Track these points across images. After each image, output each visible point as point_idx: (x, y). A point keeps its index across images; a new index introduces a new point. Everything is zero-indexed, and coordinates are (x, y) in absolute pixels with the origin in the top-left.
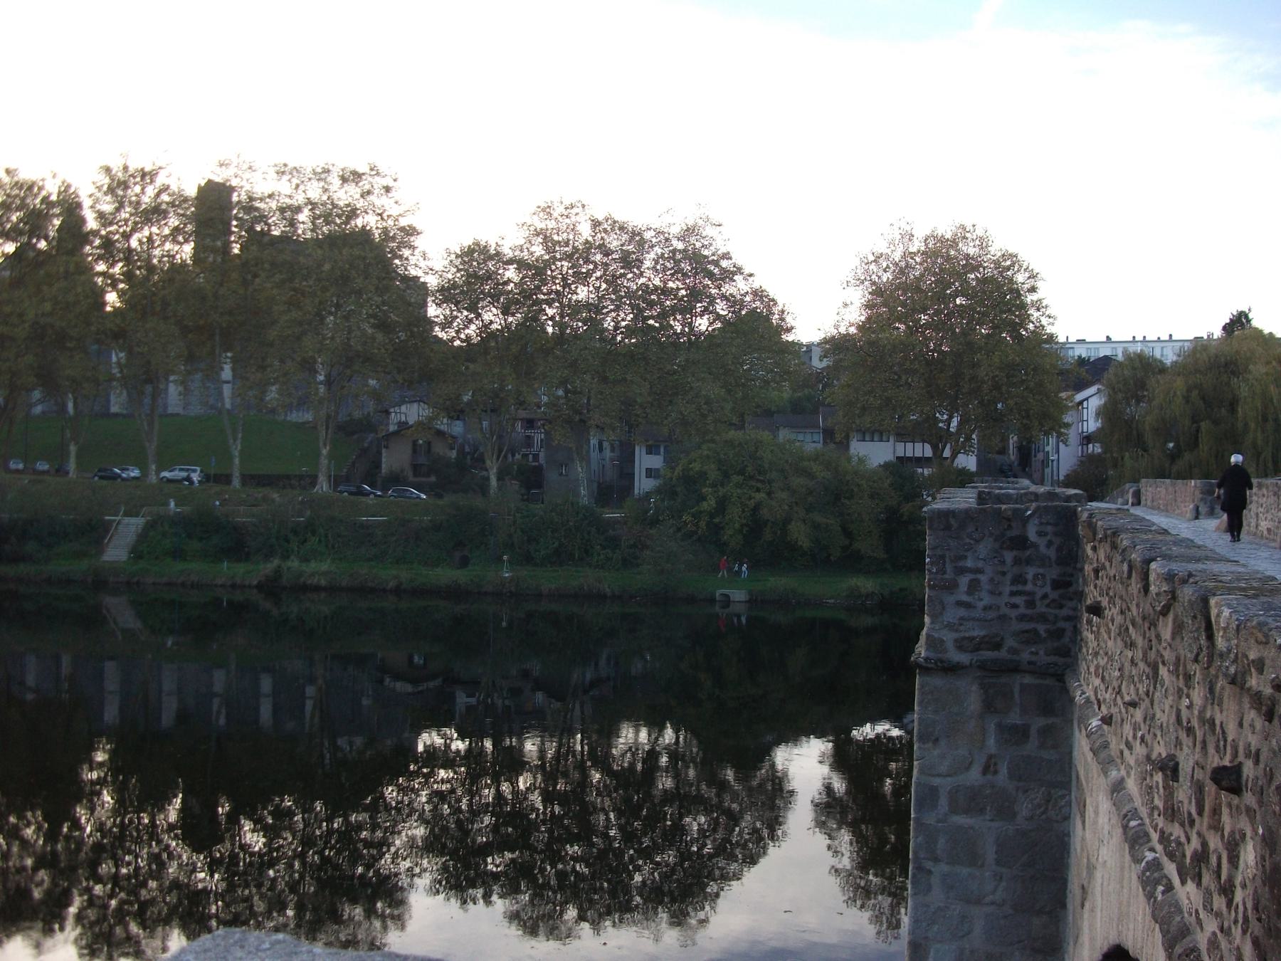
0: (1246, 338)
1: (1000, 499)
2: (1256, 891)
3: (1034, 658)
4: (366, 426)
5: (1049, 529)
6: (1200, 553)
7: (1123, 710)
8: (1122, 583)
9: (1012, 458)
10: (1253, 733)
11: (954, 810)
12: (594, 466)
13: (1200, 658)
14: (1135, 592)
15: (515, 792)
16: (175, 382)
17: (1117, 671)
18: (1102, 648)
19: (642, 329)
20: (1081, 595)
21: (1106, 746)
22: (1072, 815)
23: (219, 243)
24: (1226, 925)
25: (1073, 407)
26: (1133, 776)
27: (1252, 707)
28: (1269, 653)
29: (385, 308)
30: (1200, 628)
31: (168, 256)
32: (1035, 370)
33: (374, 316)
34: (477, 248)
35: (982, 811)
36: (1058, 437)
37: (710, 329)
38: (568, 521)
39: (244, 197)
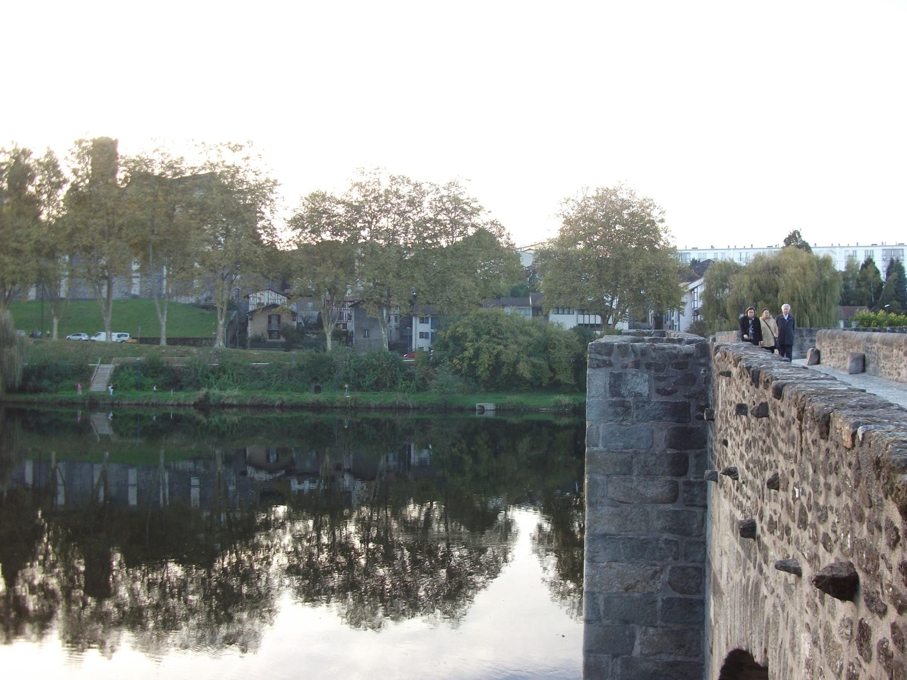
32: (663, 270)
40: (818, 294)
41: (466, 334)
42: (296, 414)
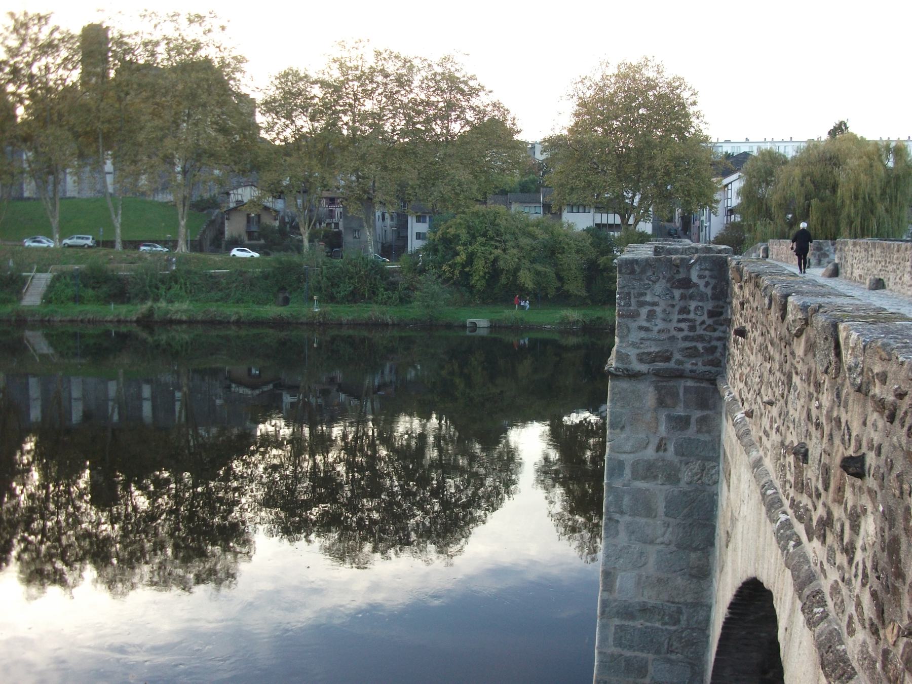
0: (845, 140)
1: (670, 252)
2: (875, 555)
3: (694, 368)
4: (213, 204)
5: (707, 273)
6: (823, 290)
7: (762, 407)
8: (763, 313)
9: (678, 225)
10: (876, 431)
11: (635, 476)
12: (379, 231)
13: (829, 370)
14: (774, 319)
15: (326, 464)
16: (70, 173)
17: (757, 378)
18: (745, 360)
19: (412, 132)
20: (729, 322)
21: (748, 433)
22: (720, 481)
23: (99, 70)
24: (847, 576)
25: (721, 188)
26: (769, 456)
27: (875, 410)
28: (892, 368)
29: (225, 117)
30: (830, 347)
31: (61, 79)
33: (216, 123)
34: (291, 72)
35: (655, 477)
36: (710, 210)
37: (462, 131)
38: (360, 271)
39: (116, 35)
40: (888, 191)
41: (459, 236)
42: (255, 331)
